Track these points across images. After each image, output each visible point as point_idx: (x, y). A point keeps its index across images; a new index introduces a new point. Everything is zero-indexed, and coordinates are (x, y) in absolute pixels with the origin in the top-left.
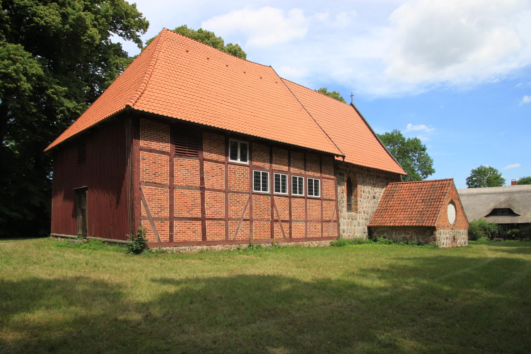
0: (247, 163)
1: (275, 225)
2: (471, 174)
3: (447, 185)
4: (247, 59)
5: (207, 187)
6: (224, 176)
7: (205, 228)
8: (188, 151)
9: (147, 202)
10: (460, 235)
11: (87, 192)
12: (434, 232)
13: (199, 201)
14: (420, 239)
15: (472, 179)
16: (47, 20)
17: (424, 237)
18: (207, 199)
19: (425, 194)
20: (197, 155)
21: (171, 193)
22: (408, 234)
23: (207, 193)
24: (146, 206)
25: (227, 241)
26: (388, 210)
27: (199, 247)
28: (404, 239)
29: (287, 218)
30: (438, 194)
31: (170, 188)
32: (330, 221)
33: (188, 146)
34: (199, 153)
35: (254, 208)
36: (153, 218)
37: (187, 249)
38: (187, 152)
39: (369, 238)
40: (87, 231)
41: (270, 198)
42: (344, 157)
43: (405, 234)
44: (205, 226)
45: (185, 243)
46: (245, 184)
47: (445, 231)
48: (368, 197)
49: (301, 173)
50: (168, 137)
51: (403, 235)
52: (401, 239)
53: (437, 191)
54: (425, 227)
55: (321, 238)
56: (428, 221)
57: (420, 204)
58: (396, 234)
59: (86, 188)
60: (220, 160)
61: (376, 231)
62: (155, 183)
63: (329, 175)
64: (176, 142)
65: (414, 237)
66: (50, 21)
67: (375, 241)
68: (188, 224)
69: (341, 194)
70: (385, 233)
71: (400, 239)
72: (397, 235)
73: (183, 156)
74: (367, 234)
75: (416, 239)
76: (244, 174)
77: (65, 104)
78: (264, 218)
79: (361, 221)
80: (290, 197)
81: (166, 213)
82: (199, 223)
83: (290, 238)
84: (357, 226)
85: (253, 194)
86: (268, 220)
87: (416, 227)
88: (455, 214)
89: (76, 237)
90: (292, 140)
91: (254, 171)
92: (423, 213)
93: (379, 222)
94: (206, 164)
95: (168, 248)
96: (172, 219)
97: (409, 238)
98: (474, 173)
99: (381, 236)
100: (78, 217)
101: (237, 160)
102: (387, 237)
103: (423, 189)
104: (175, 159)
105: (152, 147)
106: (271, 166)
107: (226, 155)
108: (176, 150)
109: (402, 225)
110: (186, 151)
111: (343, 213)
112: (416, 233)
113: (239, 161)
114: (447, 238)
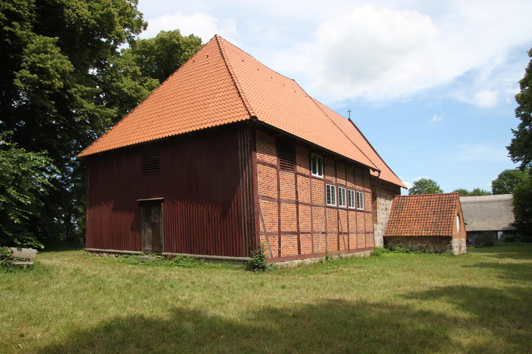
2: (413, 186)
3: (454, 199)
5: (300, 200)
8: (288, 165)
9: (263, 217)
11: (162, 204)
12: (450, 241)
14: (436, 248)
15: (414, 191)
16: (80, 13)
17: (441, 246)
19: (435, 206)
20: (293, 168)
22: (424, 243)
26: (400, 221)
28: (421, 248)
29: (346, 231)
30: (448, 207)
33: (288, 160)
36: (268, 233)
39: (385, 247)
40: (162, 246)
42: (379, 172)
43: (421, 244)
49: (352, 187)
50: (274, 150)
51: (419, 245)
52: (417, 248)
53: (446, 204)
54: (443, 237)
55: (364, 249)
56: (444, 232)
57: (432, 216)
58: (411, 243)
59: (162, 200)
61: (391, 240)
62: (268, 197)
64: (280, 155)
65: (430, 246)
66: (83, 14)
67: (392, 250)
70: (401, 242)
71: (416, 248)
72: (413, 244)
73: (285, 170)
74: (383, 243)
75: (432, 248)
77: (85, 105)
81: (275, 229)
82: (296, 237)
85: (327, 207)
87: (433, 236)
89: (142, 253)
92: (437, 224)
93: (394, 232)
97: (426, 247)
98: (416, 185)
99: (397, 245)
100: (143, 231)
102: (402, 246)
103: (431, 202)
104: (280, 172)
105: (266, 160)
106: (336, 180)
107: (310, 170)
108: (281, 163)
109: (419, 234)
110: (286, 164)
112: (432, 242)
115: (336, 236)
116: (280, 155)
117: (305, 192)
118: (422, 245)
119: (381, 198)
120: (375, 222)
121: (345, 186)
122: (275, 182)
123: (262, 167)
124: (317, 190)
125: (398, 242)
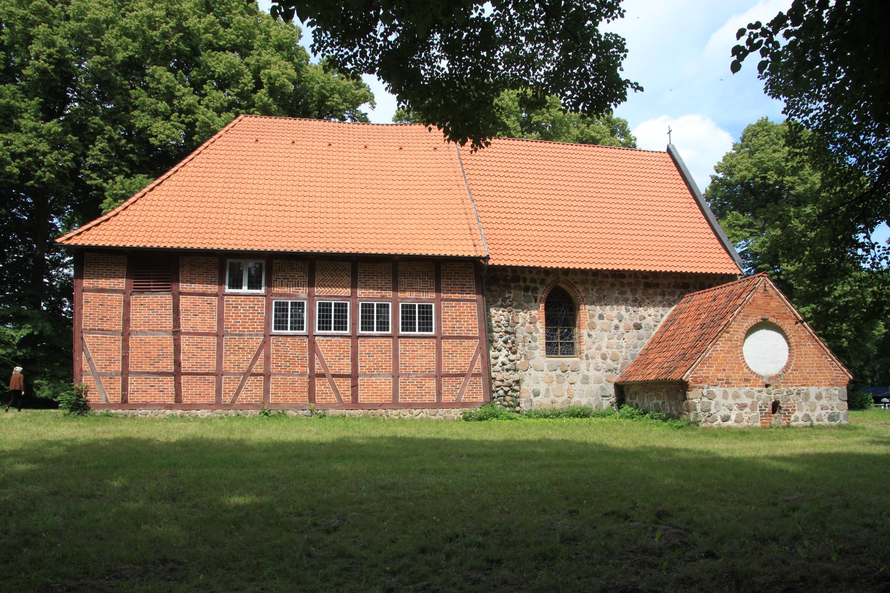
0: (262, 291)
1: (318, 382)
4: (638, 148)
6: (216, 314)
7: (181, 387)
13: (171, 349)
18: (183, 346)
21: (125, 341)
23: (184, 339)
24: (89, 359)
25: (218, 404)
27: (168, 412)
31: (122, 335)
32: (463, 375)
33: (153, 279)
34: (174, 287)
35: (273, 356)
37: (150, 414)
38: (152, 287)
41: (306, 340)
44: (180, 383)
45: (145, 405)
46: (256, 322)
48: (617, 328)
60: (209, 291)
62: (103, 330)
63: (459, 293)
68: (152, 380)
69: (527, 325)
76: (254, 307)
78: (293, 372)
79: (592, 374)
80: (395, 337)
81: (118, 367)
83: (352, 402)
84: (579, 382)
86: (302, 374)
88: (788, 351)
90: (447, 248)
91: (400, 304)
94: (183, 299)
95: (120, 411)
96: (125, 373)
101: (241, 288)
105: (100, 286)
107: (221, 283)
111: (536, 359)
113: (245, 290)
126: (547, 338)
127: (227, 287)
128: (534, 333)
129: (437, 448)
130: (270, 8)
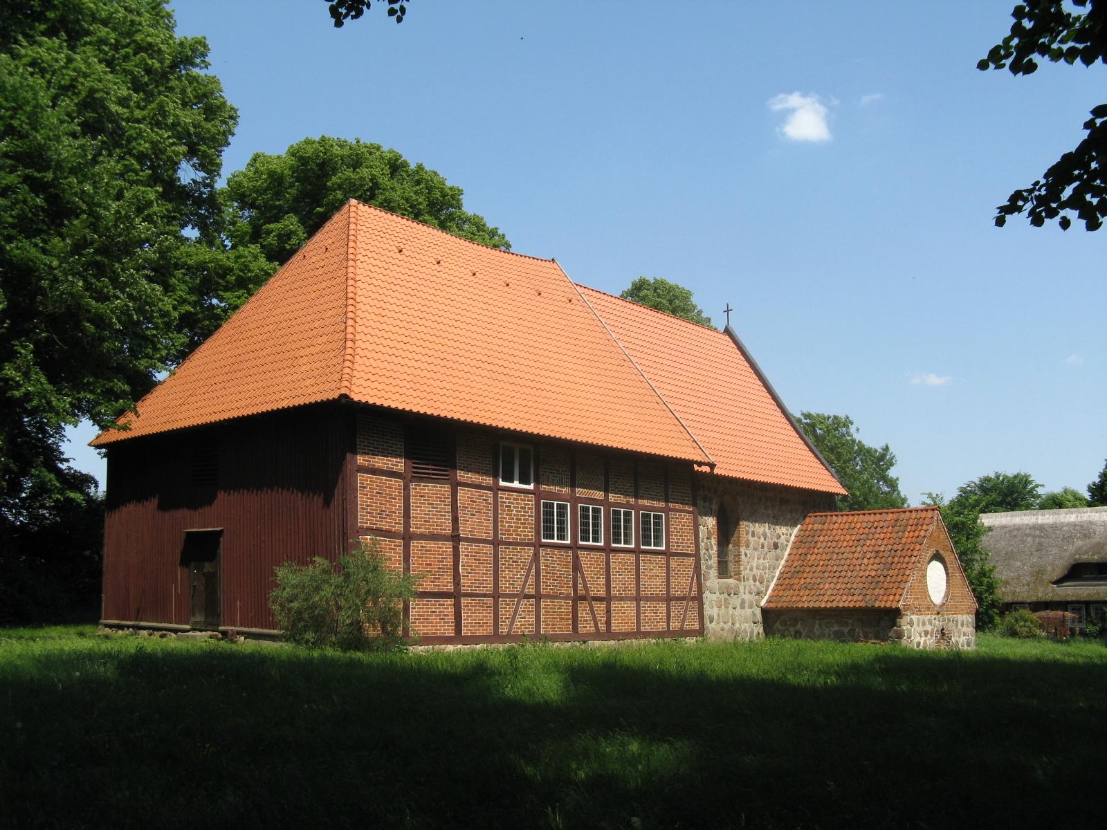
0: (531, 487)
5: (463, 534)
10: (957, 626)
22: (846, 624)
29: (602, 593)
47: (921, 618)
51: (836, 628)
58: (820, 625)
61: (779, 618)
62: (381, 530)
65: (857, 630)
70: (799, 623)
72: (824, 627)
85: (541, 546)
86: (567, 597)
89: (188, 627)
101: (513, 482)
110: (428, 469)
114: (926, 633)
115: (566, 606)
116: (409, 454)
117: (477, 519)
118: (841, 628)
119: (755, 521)
120: (736, 577)
121: (605, 502)
122: (400, 503)
123: (367, 477)
124: (514, 512)
125: (795, 621)
126: (719, 557)
127: (501, 480)
128: (710, 550)
129: (353, 625)
130: (1018, 4)
